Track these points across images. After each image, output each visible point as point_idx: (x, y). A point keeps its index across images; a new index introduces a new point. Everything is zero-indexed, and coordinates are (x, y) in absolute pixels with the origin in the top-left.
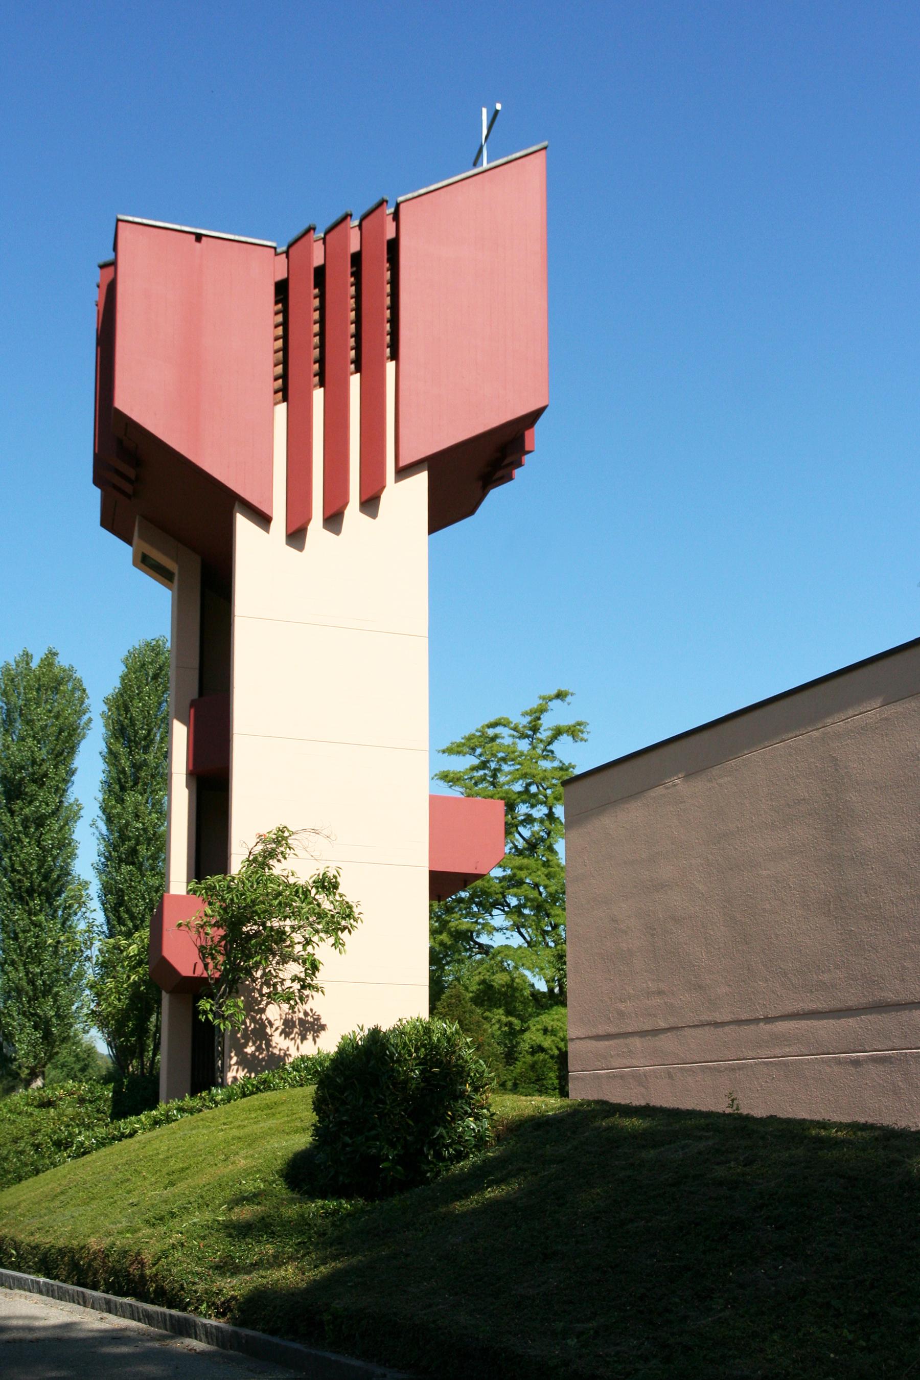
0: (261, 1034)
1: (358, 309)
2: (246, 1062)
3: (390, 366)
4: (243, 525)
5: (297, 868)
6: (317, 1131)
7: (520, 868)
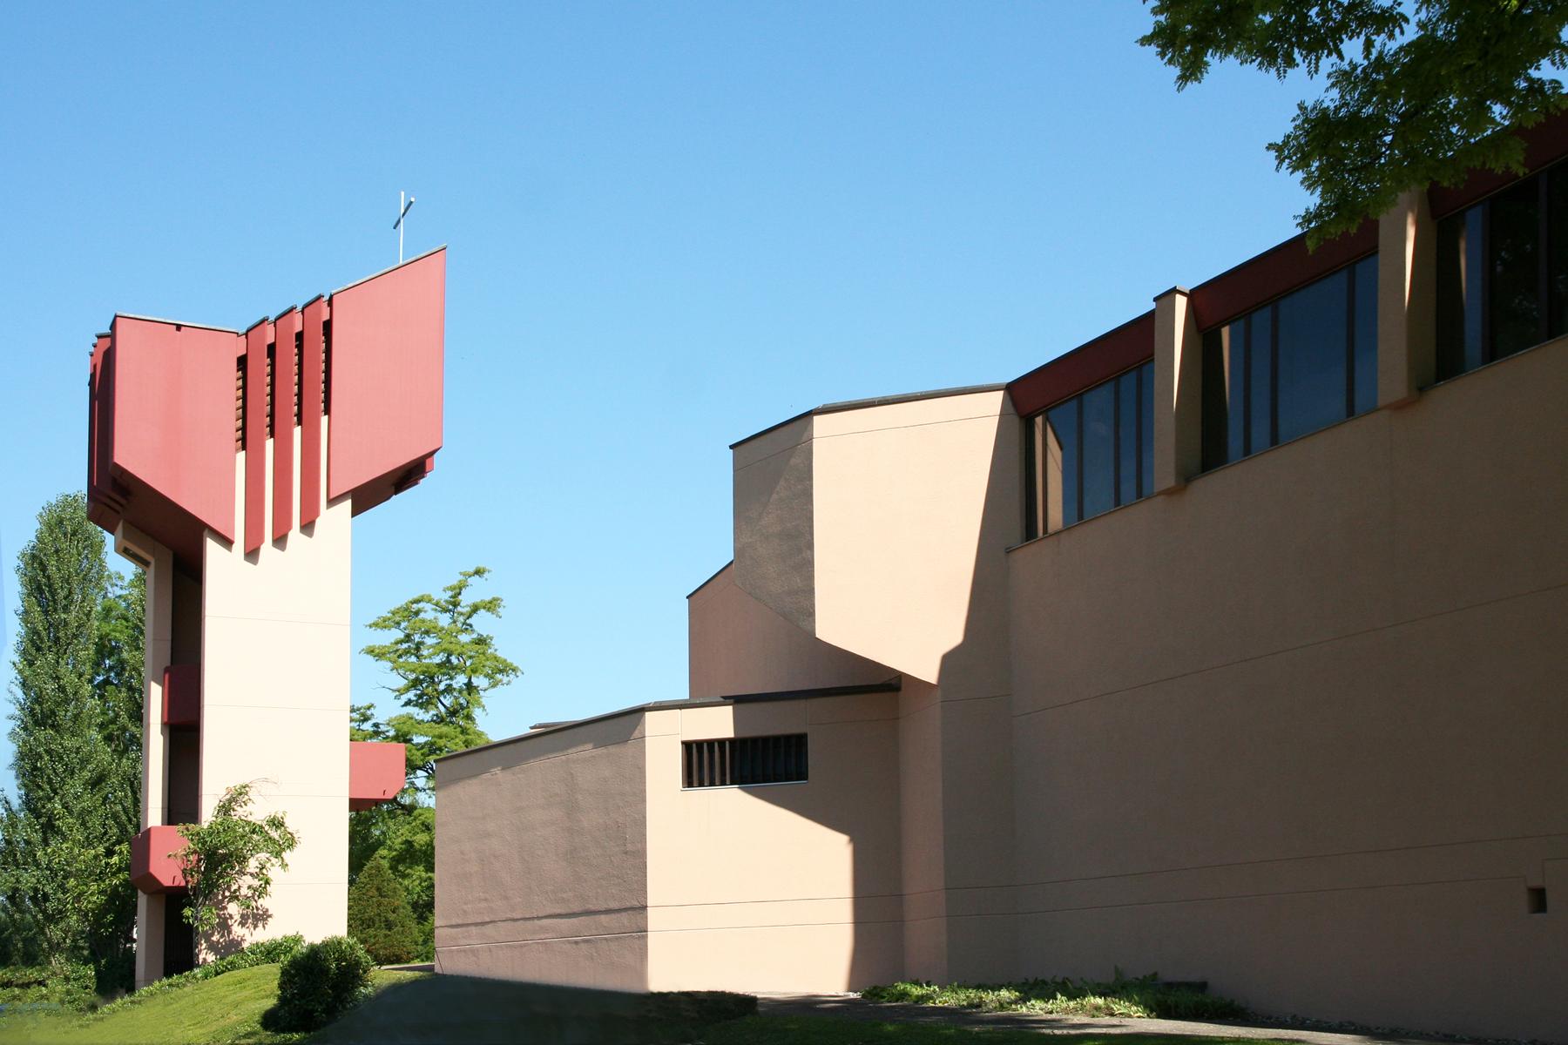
0: (224, 926)
1: (300, 374)
2: (212, 947)
3: (324, 419)
4: (212, 548)
5: (256, 811)
6: (280, 998)
7: (440, 737)
